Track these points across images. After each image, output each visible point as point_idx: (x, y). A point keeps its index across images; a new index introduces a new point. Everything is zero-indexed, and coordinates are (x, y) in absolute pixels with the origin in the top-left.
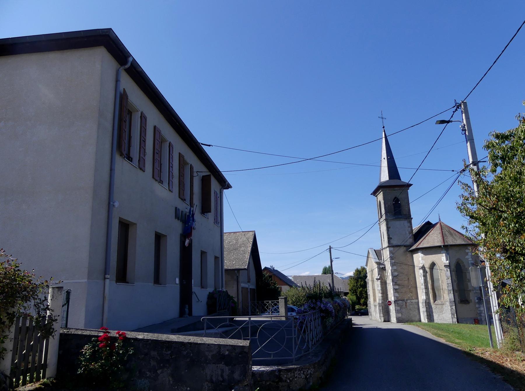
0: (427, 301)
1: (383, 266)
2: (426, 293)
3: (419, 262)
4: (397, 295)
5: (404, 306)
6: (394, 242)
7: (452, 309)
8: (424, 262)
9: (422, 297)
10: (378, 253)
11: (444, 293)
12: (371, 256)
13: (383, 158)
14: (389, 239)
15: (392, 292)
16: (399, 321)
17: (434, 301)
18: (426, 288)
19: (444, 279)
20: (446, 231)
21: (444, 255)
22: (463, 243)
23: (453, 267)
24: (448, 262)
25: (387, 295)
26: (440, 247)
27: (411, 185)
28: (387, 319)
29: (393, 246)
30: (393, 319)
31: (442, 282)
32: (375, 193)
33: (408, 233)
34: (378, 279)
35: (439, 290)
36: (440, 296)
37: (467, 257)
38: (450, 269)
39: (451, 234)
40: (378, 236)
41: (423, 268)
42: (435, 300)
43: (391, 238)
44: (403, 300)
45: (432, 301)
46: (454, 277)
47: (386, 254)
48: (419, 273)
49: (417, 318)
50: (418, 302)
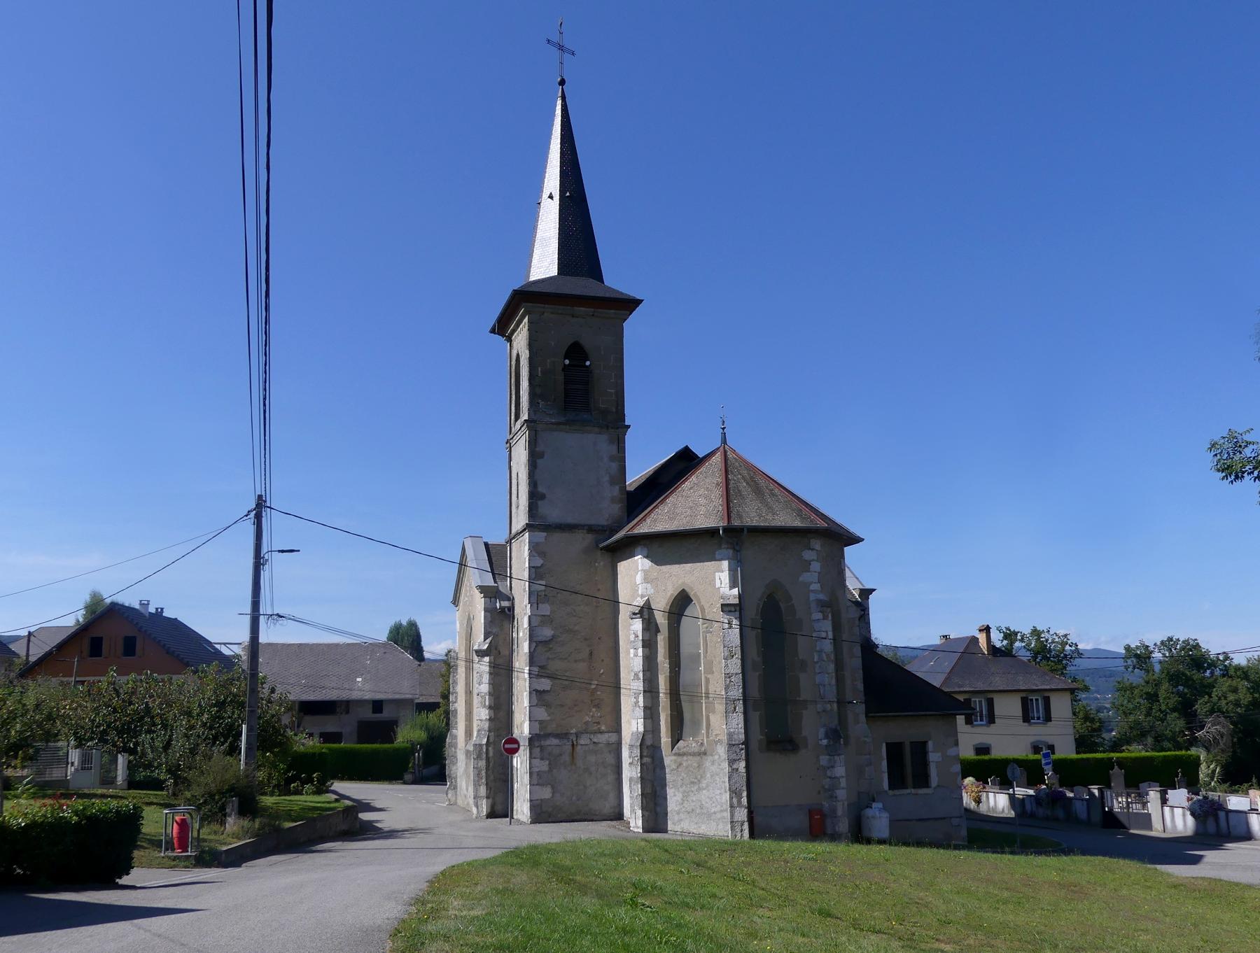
0: (649, 742)
1: (506, 604)
2: (645, 707)
3: (634, 587)
4: (542, 714)
5: (567, 758)
6: (553, 513)
7: (733, 772)
8: (651, 591)
9: (632, 724)
10: (496, 558)
11: (711, 709)
12: (471, 561)
13: (545, 195)
14: (535, 497)
15: (526, 703)
16: (541, 814)
17: (674, 744)
18: (650, 690)
19: (717, 653)
20: (740, 478)
21: (725, 564)
22: (797, 523)
23: (752, 612)
24: (735, 591)
25: (510, 714)
26: (712, 532)
27: (1247, 836)
28: (500, 809)
29: (548, 528)
30: (522, 808)
31: (709, 670)
32: (503, 327)
33: (606, 478)
34: (481, 653)
35: (695, 698)
36: (696, 724)
37: (805, 577)
38: (741, 619)
39: (758, 491)
40: (493, 485)
41: (646, 613)
42: (677, 736)
43: (543, 497)
44: (563, 736)
45: (665, 739)
46: (753, 653)
47: (521, 558)
48: (631, 630)
49: (608, 807)
50: (619, 744)
